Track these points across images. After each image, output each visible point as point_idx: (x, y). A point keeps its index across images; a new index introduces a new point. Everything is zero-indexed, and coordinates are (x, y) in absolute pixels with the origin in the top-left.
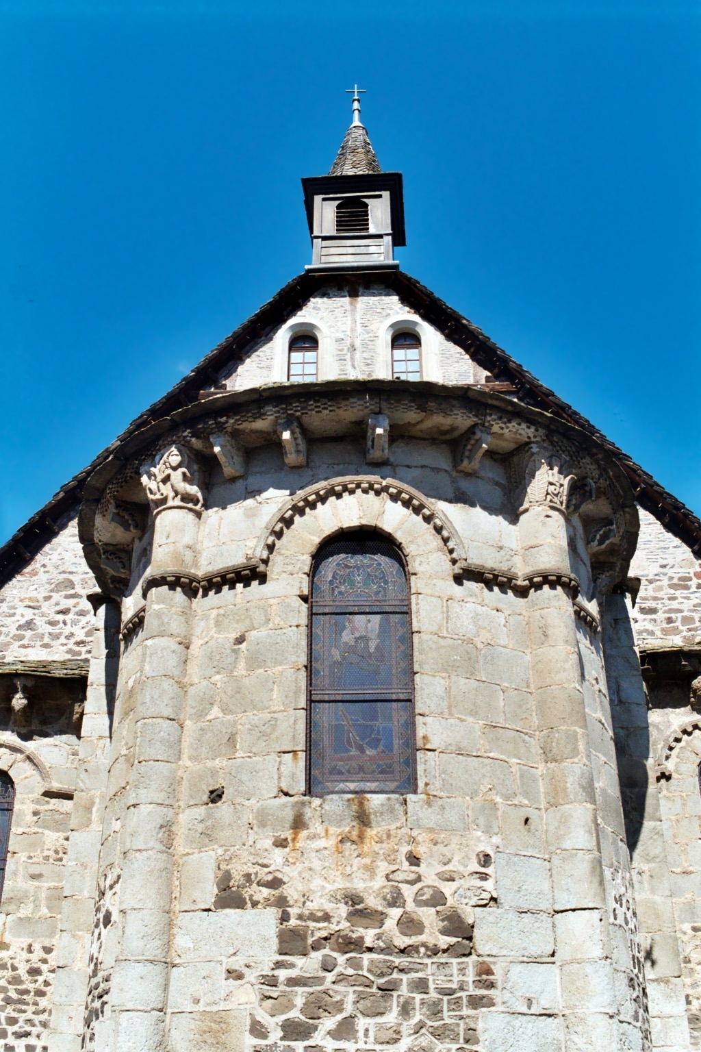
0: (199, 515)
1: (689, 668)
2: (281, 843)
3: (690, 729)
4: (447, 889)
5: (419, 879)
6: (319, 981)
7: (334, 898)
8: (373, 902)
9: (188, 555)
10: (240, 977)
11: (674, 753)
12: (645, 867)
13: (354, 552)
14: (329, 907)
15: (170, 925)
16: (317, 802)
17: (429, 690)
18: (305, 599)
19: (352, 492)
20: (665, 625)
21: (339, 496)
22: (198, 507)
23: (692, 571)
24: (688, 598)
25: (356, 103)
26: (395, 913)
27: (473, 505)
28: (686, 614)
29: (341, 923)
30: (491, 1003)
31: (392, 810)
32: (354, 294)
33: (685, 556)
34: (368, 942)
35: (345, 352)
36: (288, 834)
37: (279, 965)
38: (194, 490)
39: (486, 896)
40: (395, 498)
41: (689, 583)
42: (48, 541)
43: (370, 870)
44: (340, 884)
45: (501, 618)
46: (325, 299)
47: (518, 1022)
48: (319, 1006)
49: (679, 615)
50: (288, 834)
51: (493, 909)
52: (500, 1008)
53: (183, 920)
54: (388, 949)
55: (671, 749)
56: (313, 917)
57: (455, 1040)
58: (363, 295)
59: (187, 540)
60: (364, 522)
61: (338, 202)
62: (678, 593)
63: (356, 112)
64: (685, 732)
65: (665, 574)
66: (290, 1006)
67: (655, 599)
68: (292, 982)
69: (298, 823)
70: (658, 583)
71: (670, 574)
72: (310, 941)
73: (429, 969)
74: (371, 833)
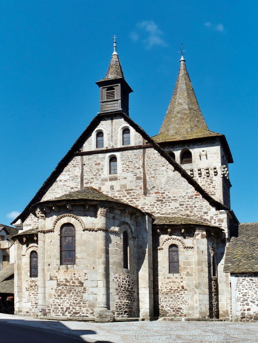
0: (45, 219)
1: (166, 227)
2: (57, 272)
3: (167, 239)
4: (79, 278)
5: (75, 277)
6: (62, 290)
7: (63, 279)
8: (68, 280)
9: (44, 227)
10: (53, 289)
11: (164, 244)
12: (144, 269)
13: (67, 226)
14: (63, 280)
15: (45, 282)
16: (61, 266)
17: (78, 249)
18: (59, 235)
19: (66, 217)
20: (185, 208)
21: (64, 217)
22: (44, 218)
23: (194, 194)
24: (192, 201)
25: (115, 43)
26: (72, 281)
27: (88, 216)
28: (191, 205)
29: (64, 283)
30: (85, 293)
31: (71, 267)
32: (112, 119)
33: (193, 190)
34: (68, 285)
35: (110, 138)
36: (58, 271)
37: (57, 288)
38: (43, 215)
39: (86, 279)
40: (73, 217)
41: (193, 197)
42: (44, 194)
43: (68, 275)
44: (64, 277)
45: (92, 236)
46: (105, 121)
47: (90, 295)
48: (62, 293)
49: (189, 206)
50: (58, 271)
51: (87, 280)
52: (87, 293)
53: (46, 282)
54: (71, 286)
55: (164, 243)
56: (61, 282)
57: (80, 297)
58: (114, 119)
59: (43, 224)
60: (68, 222)
61: (107, 89)
62: (190, 200)
63: (115, 47)
64: (166, 240)
65: (187, 195)
66: (58, 293)
67: (184, 202)
68: (58, 290)
69: (59, 269)
70: (185, 198)
71: (188, 195)
72: (61, 285)
73: (76, 288)
74: (68, 270)
